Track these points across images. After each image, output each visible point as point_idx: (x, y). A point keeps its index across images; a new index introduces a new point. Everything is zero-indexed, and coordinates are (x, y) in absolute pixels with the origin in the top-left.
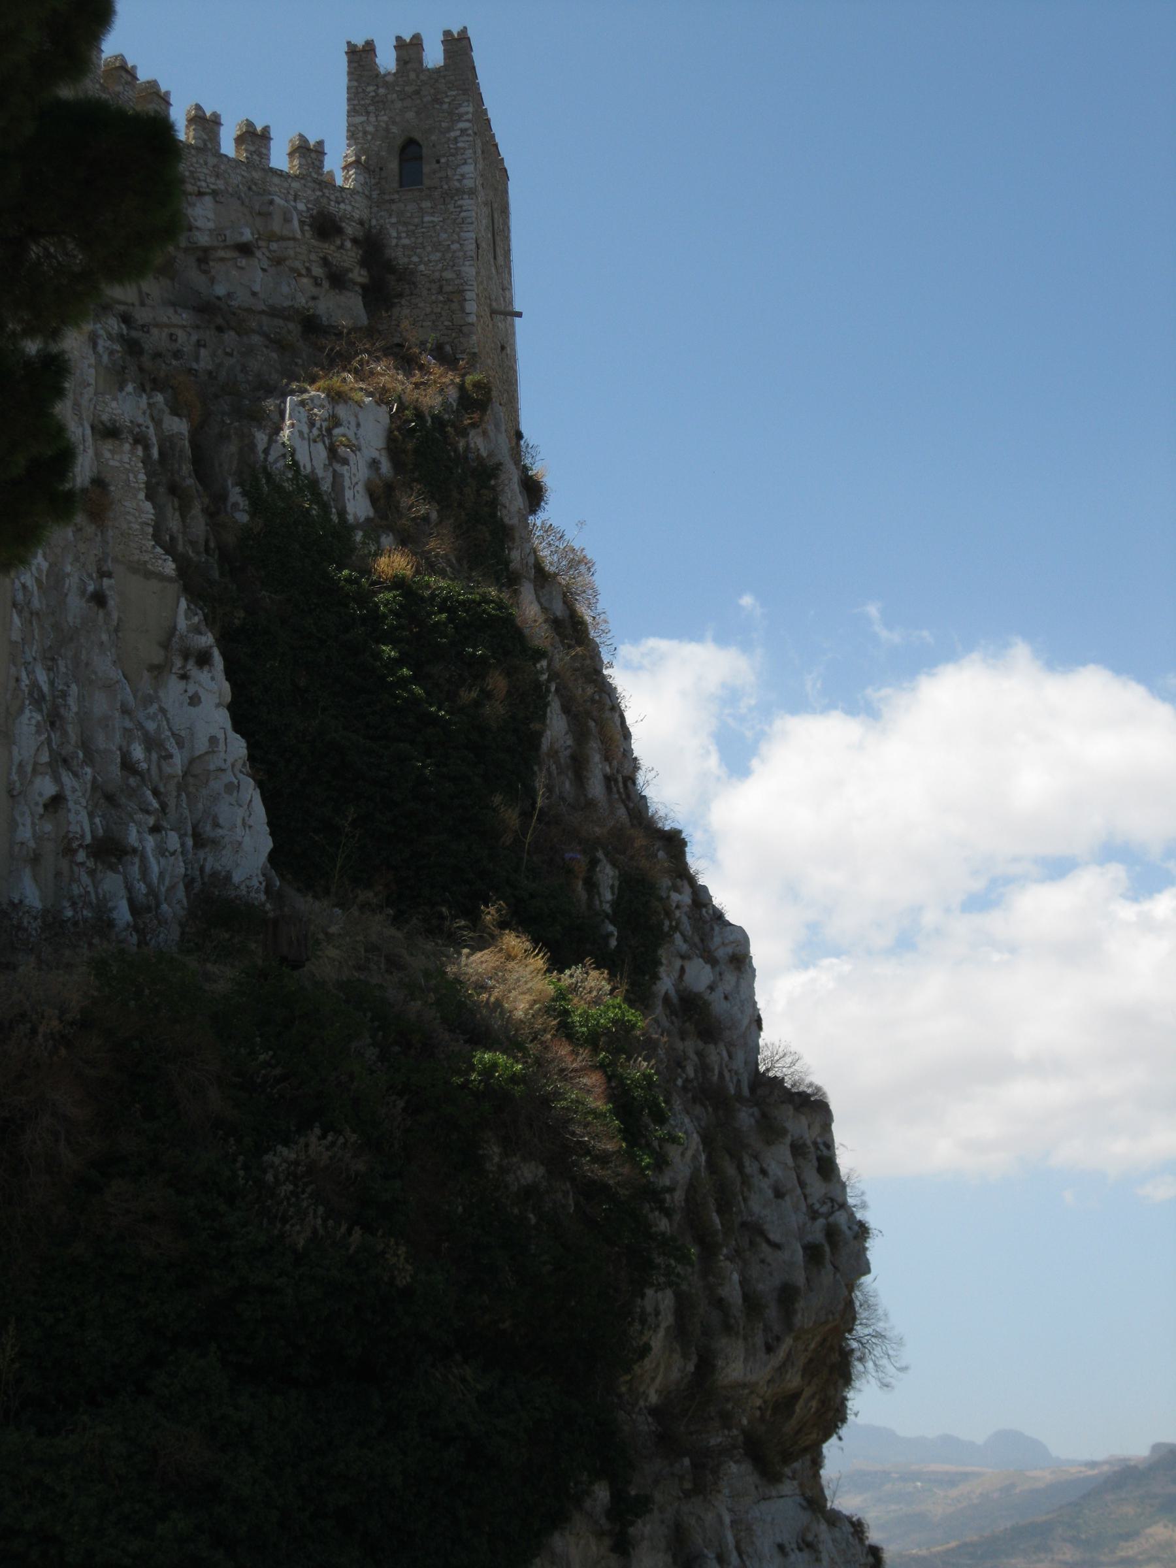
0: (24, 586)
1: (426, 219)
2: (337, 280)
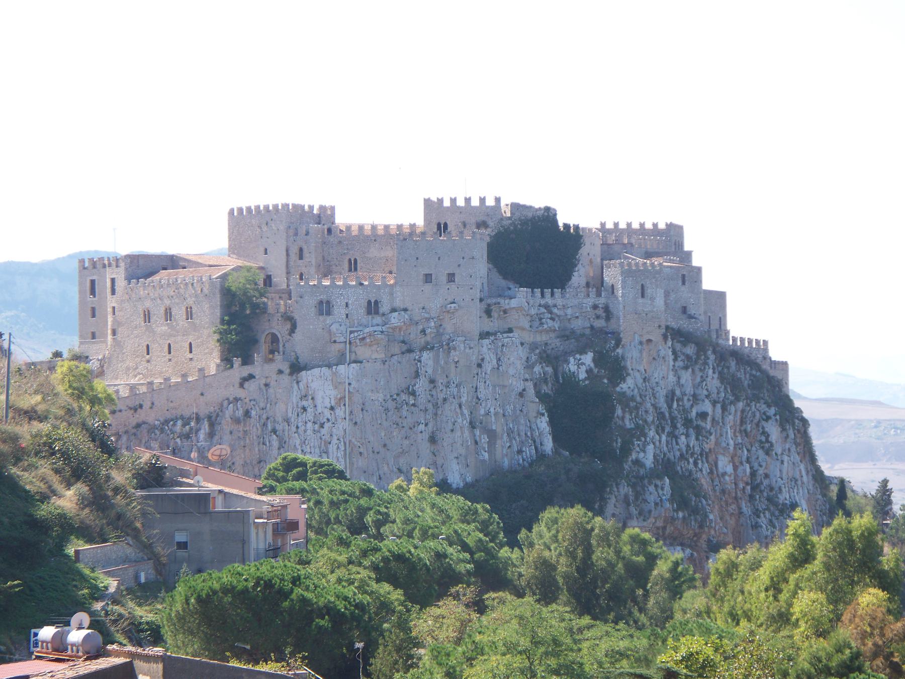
2: (598, 317)
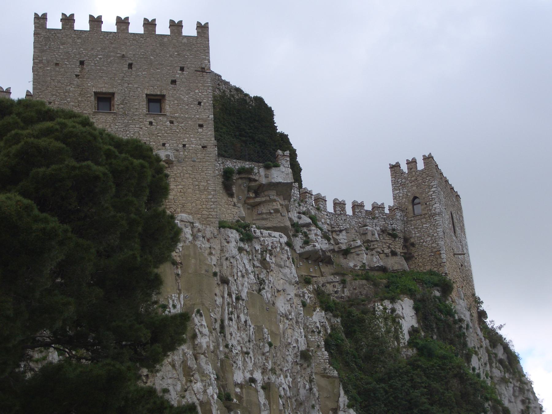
0: (284, 389)
1: (424, 226)
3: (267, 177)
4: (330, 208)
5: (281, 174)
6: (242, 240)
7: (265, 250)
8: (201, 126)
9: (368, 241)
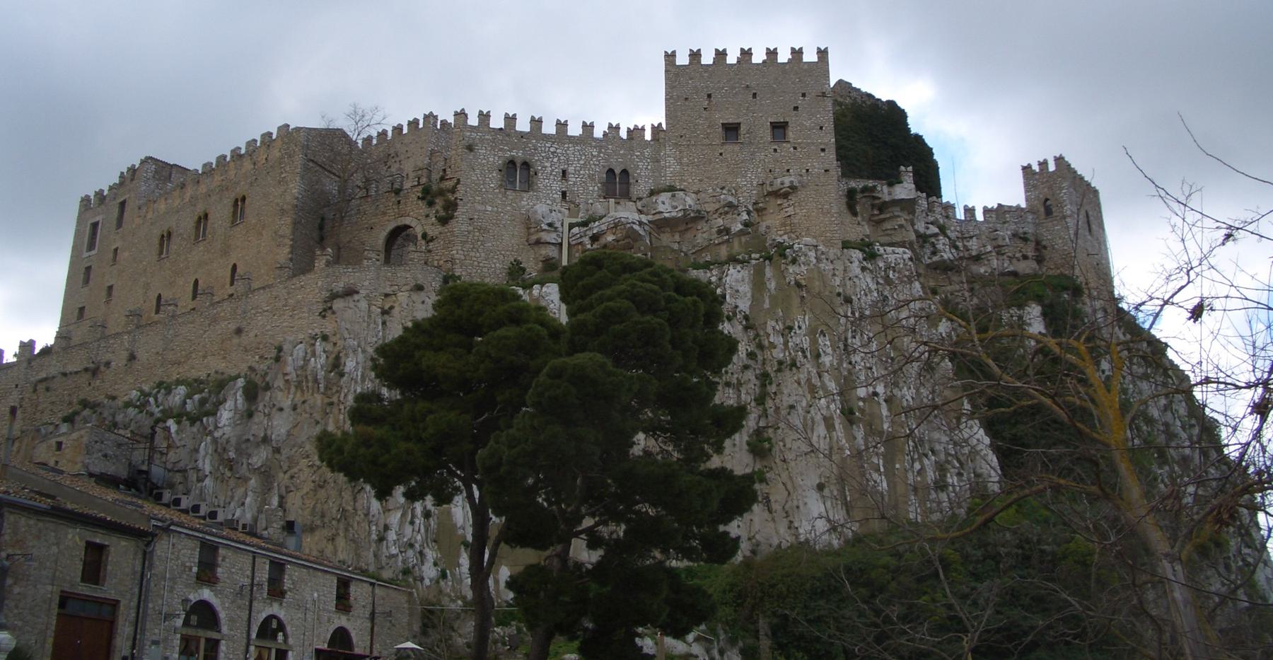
3: (890, 194)
4: (960, 215)
5: (905, 189)
6: (865, 259)
7: (888, 267)
8: (823, 150)
9: (999, 246)
